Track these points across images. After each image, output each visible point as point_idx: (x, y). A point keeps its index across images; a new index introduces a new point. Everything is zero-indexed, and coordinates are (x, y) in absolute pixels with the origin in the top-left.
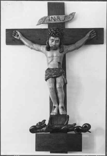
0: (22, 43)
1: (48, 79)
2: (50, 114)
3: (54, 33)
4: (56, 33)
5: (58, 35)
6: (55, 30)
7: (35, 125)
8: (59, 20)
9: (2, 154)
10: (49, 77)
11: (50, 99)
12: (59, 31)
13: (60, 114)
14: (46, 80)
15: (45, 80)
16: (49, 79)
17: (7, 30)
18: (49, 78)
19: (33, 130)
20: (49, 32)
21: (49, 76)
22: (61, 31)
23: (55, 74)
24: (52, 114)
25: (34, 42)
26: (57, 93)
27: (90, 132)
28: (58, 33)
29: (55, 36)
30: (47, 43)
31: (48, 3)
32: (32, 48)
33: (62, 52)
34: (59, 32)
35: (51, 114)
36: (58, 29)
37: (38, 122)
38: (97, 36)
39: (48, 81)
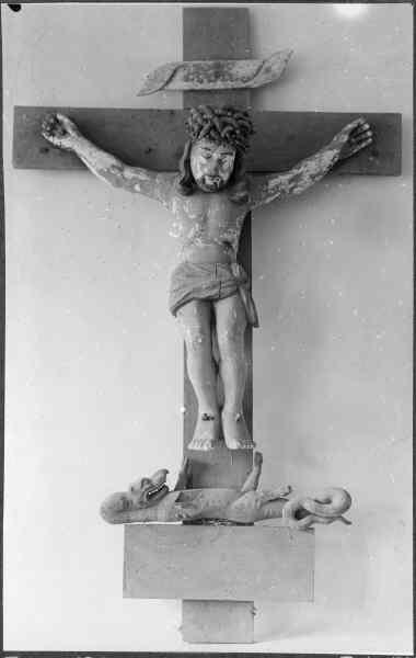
0: (75, 162)
1: (184, 304)
2: (185, 448)
3: (214, 127)
4: (225, 124)
5: (232, 133)
6: (219, 116)
7: (125, 489)
8: (292, 185)
9: (409, 8)
10: (191, 296)
11: (187, 382)
12: (235, 116)
13: (229, 450)
14: (175, 311)
15: (170, 313)
16: (188, 305)
17: (19, 110)
18: (189, 301)
19: (120, 510)
20: (196, 122)
21: (188, 294)
22: (241, 119)
23: (214, 287)
24: (196, 448)
25: (127, 158)
26: (216, 366)
27: (348, 523)
28: (232, 125)
29: (213, 134)
30: (182, 166)
31: (186, 11)
32: (118, 183)
33: (241, 205)
34: (234, 123)
35: (190, 447)
36: (229, 110)
37: (135, 479)
38: (374, 142)
39: (178, 314)
